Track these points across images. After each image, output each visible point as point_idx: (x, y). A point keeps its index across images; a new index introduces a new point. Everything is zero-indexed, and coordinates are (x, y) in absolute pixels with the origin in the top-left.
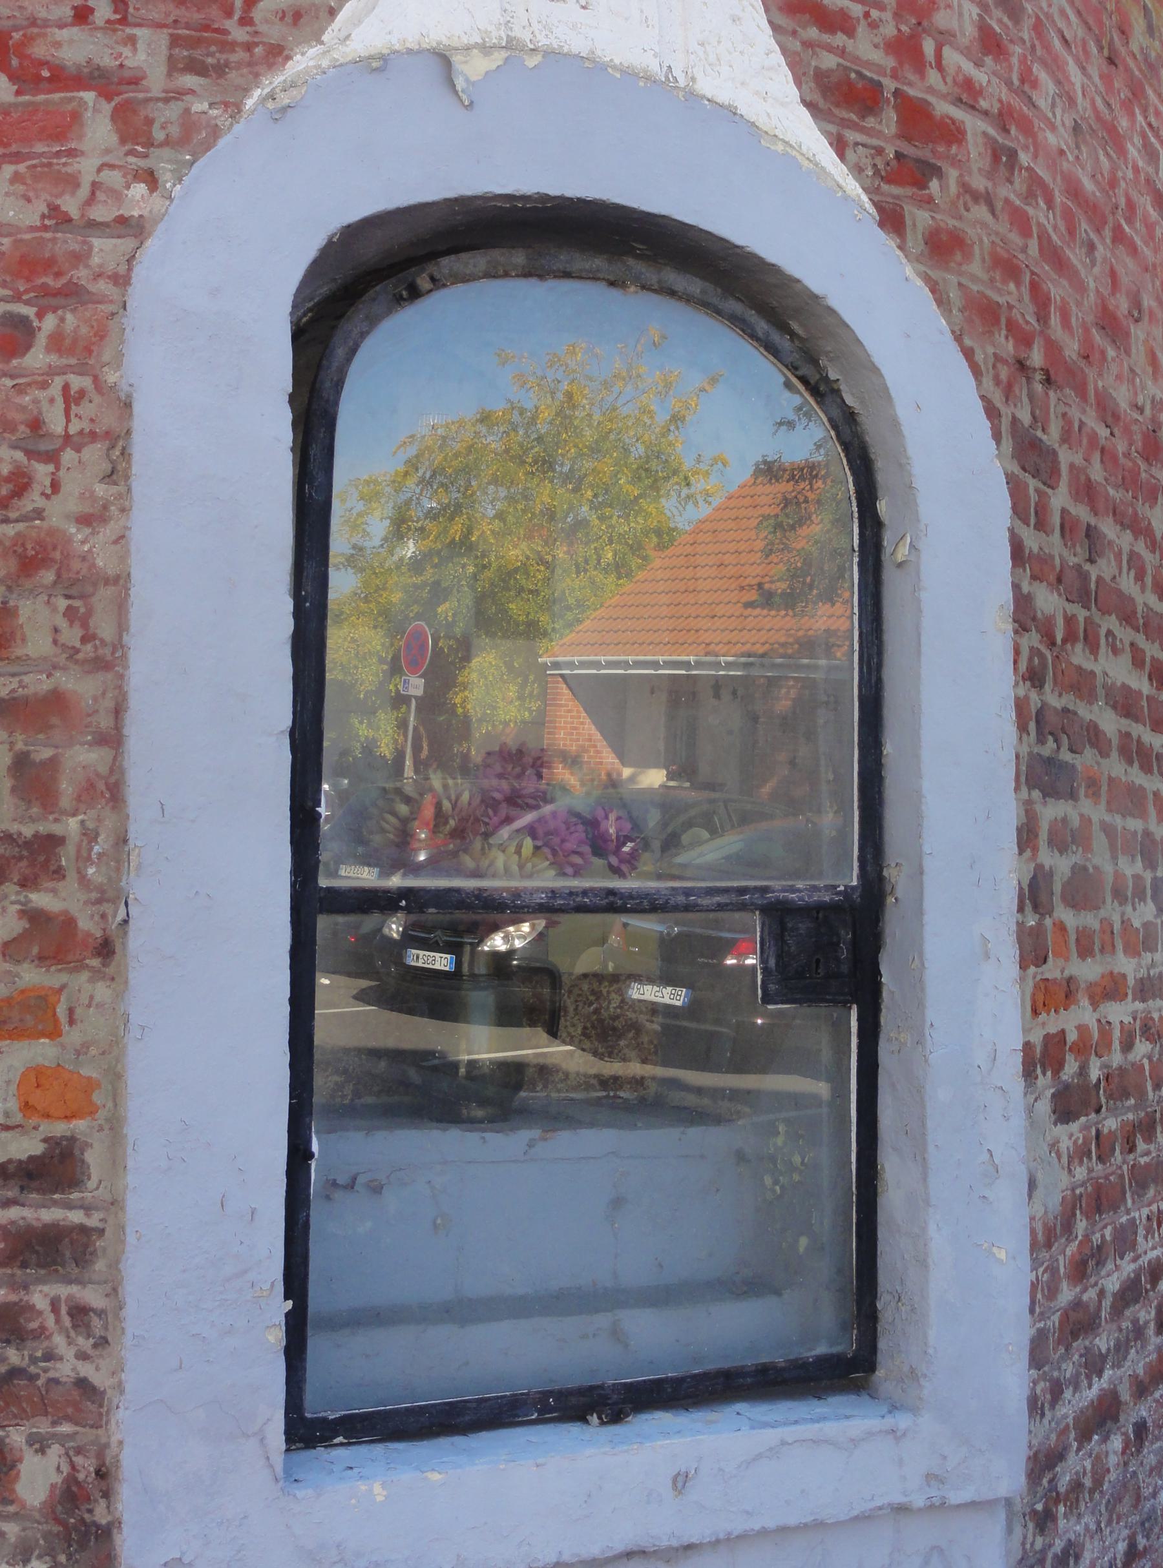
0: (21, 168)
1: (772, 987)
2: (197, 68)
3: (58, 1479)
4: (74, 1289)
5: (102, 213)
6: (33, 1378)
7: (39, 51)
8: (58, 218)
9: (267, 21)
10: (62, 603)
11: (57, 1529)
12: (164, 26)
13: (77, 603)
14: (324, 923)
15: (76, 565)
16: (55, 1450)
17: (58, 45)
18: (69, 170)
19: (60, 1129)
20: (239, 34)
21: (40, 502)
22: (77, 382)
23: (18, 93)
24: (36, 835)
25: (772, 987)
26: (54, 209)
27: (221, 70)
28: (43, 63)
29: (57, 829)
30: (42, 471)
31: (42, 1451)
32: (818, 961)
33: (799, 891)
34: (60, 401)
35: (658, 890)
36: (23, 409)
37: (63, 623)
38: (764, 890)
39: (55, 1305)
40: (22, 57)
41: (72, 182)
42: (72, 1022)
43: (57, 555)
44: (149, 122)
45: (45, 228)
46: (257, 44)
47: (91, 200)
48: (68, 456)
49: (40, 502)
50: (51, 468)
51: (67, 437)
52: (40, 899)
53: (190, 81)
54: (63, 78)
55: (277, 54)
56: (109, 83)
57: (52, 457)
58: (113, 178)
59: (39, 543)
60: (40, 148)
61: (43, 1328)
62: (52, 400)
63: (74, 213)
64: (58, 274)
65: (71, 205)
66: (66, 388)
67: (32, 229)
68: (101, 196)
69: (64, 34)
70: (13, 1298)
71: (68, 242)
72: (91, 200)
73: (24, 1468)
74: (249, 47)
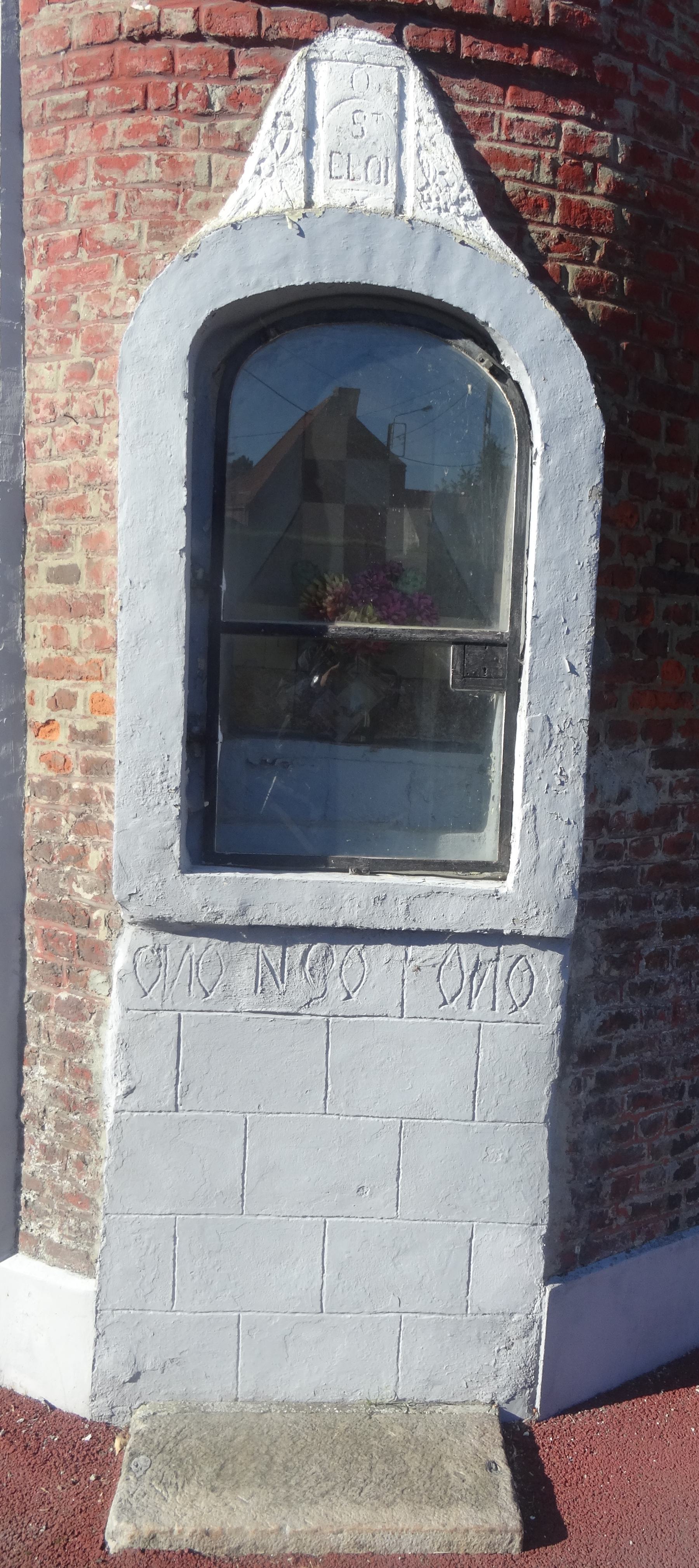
0: (90, 293)
1: (458, 680)
2: (161, 237)
3: (101, 860)
4: (107, 785)
5: (117, 312)
6: (94, 819)
7: (97, 236)
8: (102, 315)
9: (193, 210)
10: (103, 492)
11: (101, 879)
12: (147, 218)
13: (108, 493)
14: (224, 639)
15: (108, 475)
16: (101, 848)
17: (103, 232)
18: (107, 292)
19: (102, 718)
20: (179, 218)
21: (96, 448)
22: (108, 392)
23: (89, 257)
24: (94, 594)
25: (458, 680)
26: (101, 311)
27: (171, 236)
28: (98, 243)
29: (101, 592)
30: (96, 433)
31: (96, 848)
32: (485, 669)
33: (474, 633)
34: (102, 402)
35: (395, 630)
36: (89, 405)
37: (103, 501)
38: (455, 632)
39: (101, 790)
40: (90, 239)
41: (107, 298)
42: (106, 675)
43: (101, 471)
44: (138, 266)
45: (98, 321)
46: (187, 222)
47: (114, 306)
48: (105, 426)
49: (96, 448)
50: (99, 432)
51: (104, 417)
52: (96, 622)
53: (157, 244)
54: (106, 249)
55: (197, 224)
56: (121, 248)
57: (99, 427)
58: (122, 294)
59: (96, 466)
60: (97, 282)
61: (97, 800)
62: (99, 401)
63: (108, 313)
64: (102, 342)
65: (106, 309)
66: (104, 395)
67: (94, 321)
68: (117, 304)
69: (105, 227)
70: (87, 787)
71: (105, 327)
72: (114, 306)
73: (91, 855)
74: (183, 223)
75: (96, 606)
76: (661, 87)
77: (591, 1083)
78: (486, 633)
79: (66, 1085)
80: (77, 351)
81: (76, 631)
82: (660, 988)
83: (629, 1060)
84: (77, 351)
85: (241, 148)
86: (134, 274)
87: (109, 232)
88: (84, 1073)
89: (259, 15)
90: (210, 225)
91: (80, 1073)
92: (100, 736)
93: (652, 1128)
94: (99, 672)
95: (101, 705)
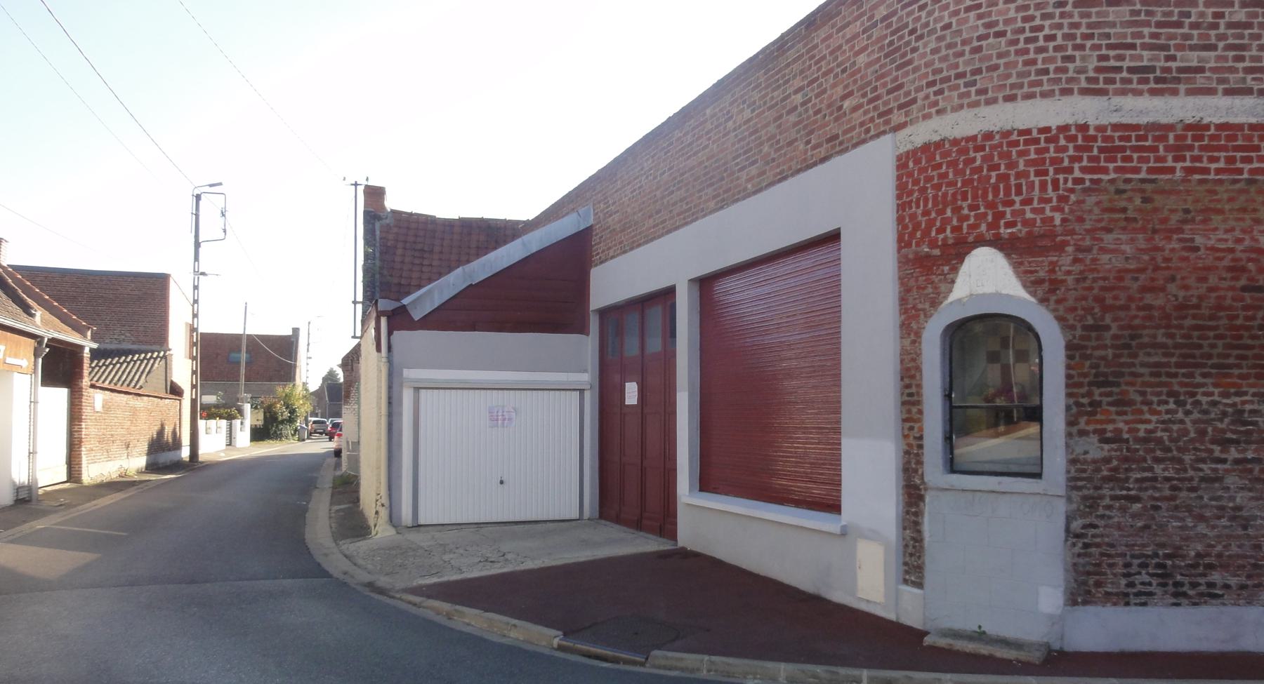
56: (924, 310)
75: (919, 403)
76: (1083, 239)
77: (1080, 545)
78: (667, 658)
79: (914, 535)
80: (912, 337)
81: (914, 410)
82: (1110, 517)
83: (1098, 540)
84: (912, 337)
85: (953, 282)
86: (926, 316)
87: (920, 306)
88: (919, 532)
89: (912, 564)
90: (946, 302)
91: (913, 561)
92: (921, 438)
93: (1111, 566)
94: (919, 420)
95: (921, 429)
